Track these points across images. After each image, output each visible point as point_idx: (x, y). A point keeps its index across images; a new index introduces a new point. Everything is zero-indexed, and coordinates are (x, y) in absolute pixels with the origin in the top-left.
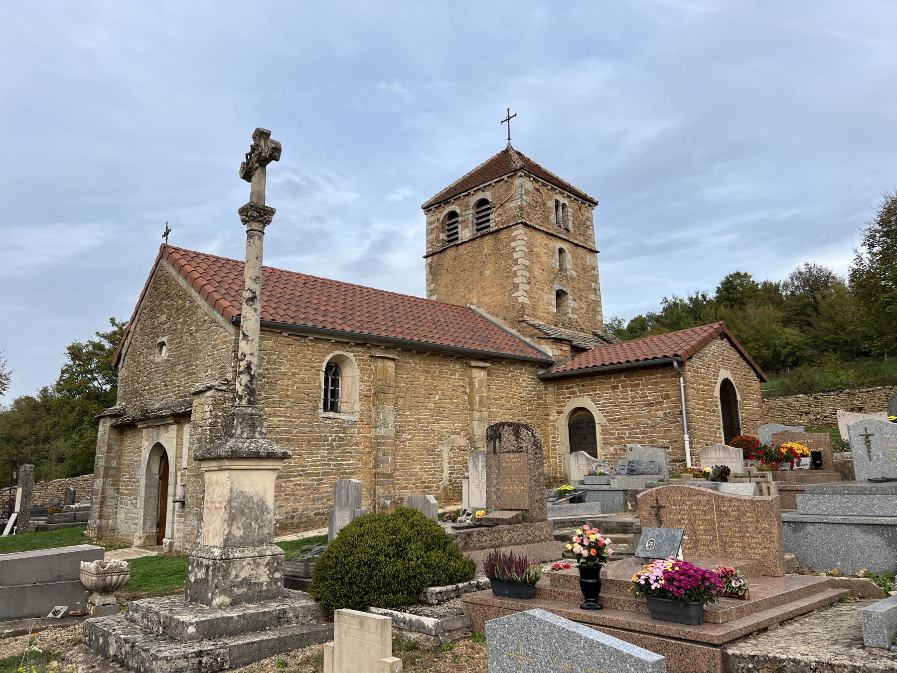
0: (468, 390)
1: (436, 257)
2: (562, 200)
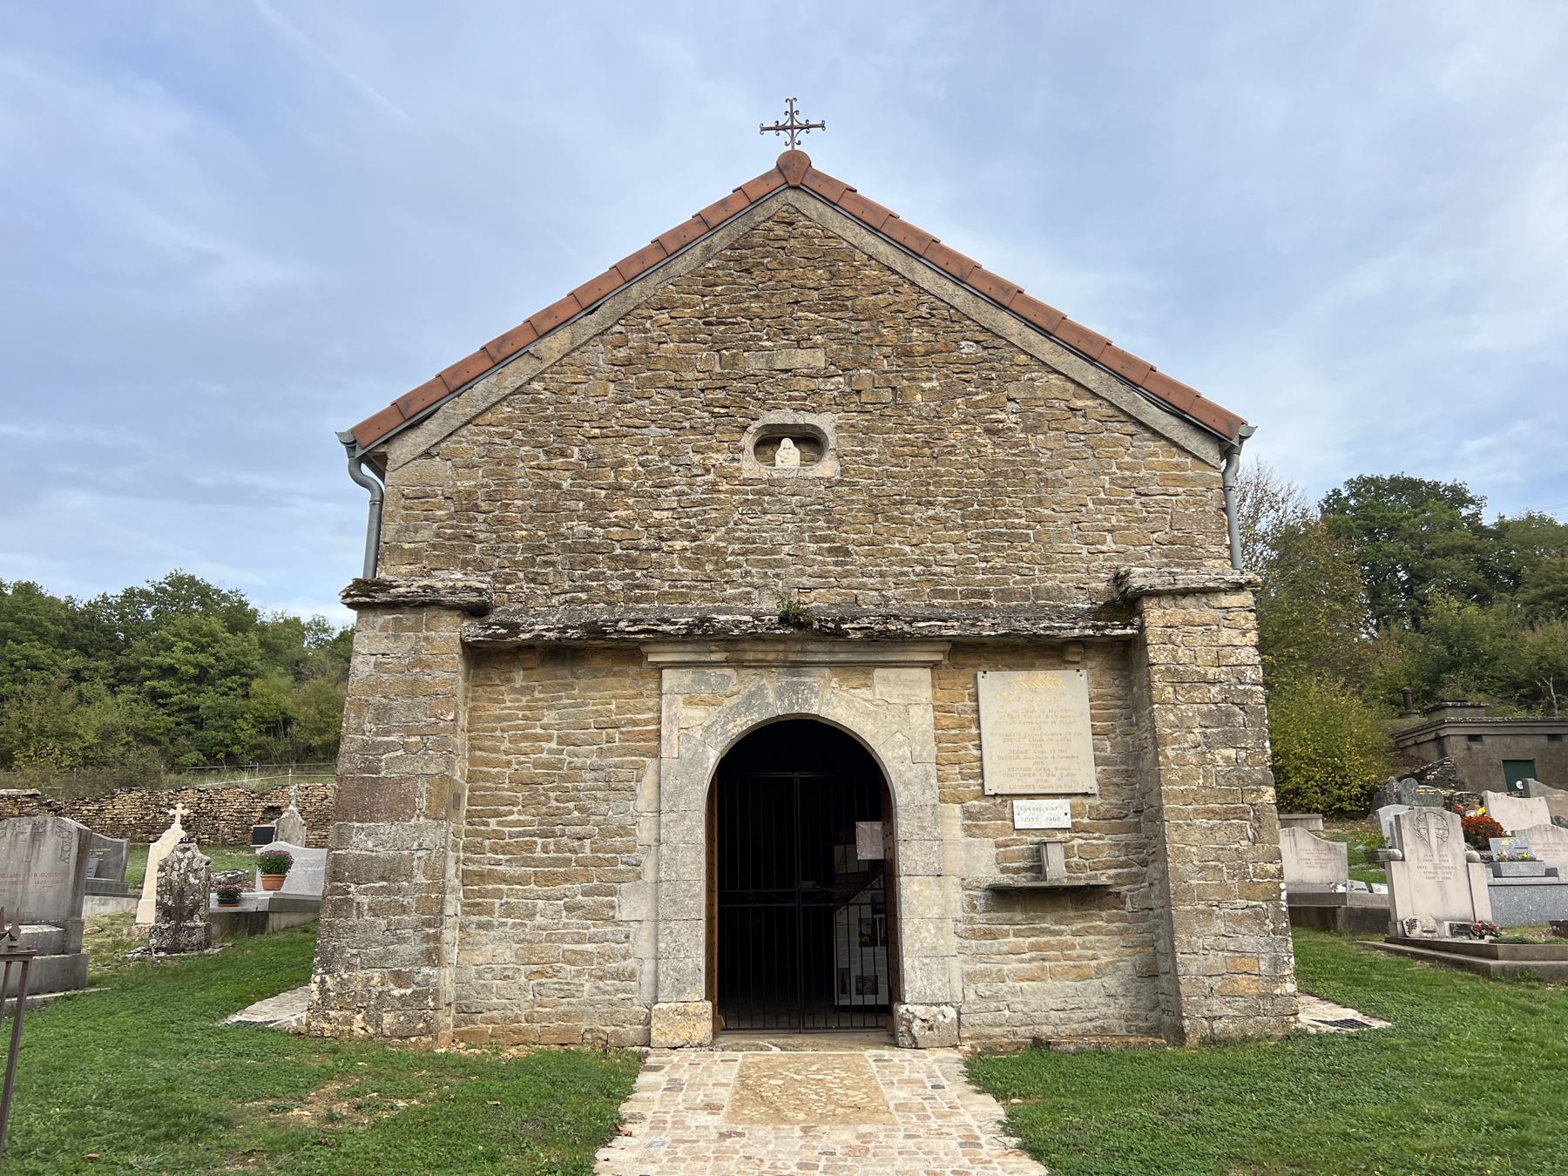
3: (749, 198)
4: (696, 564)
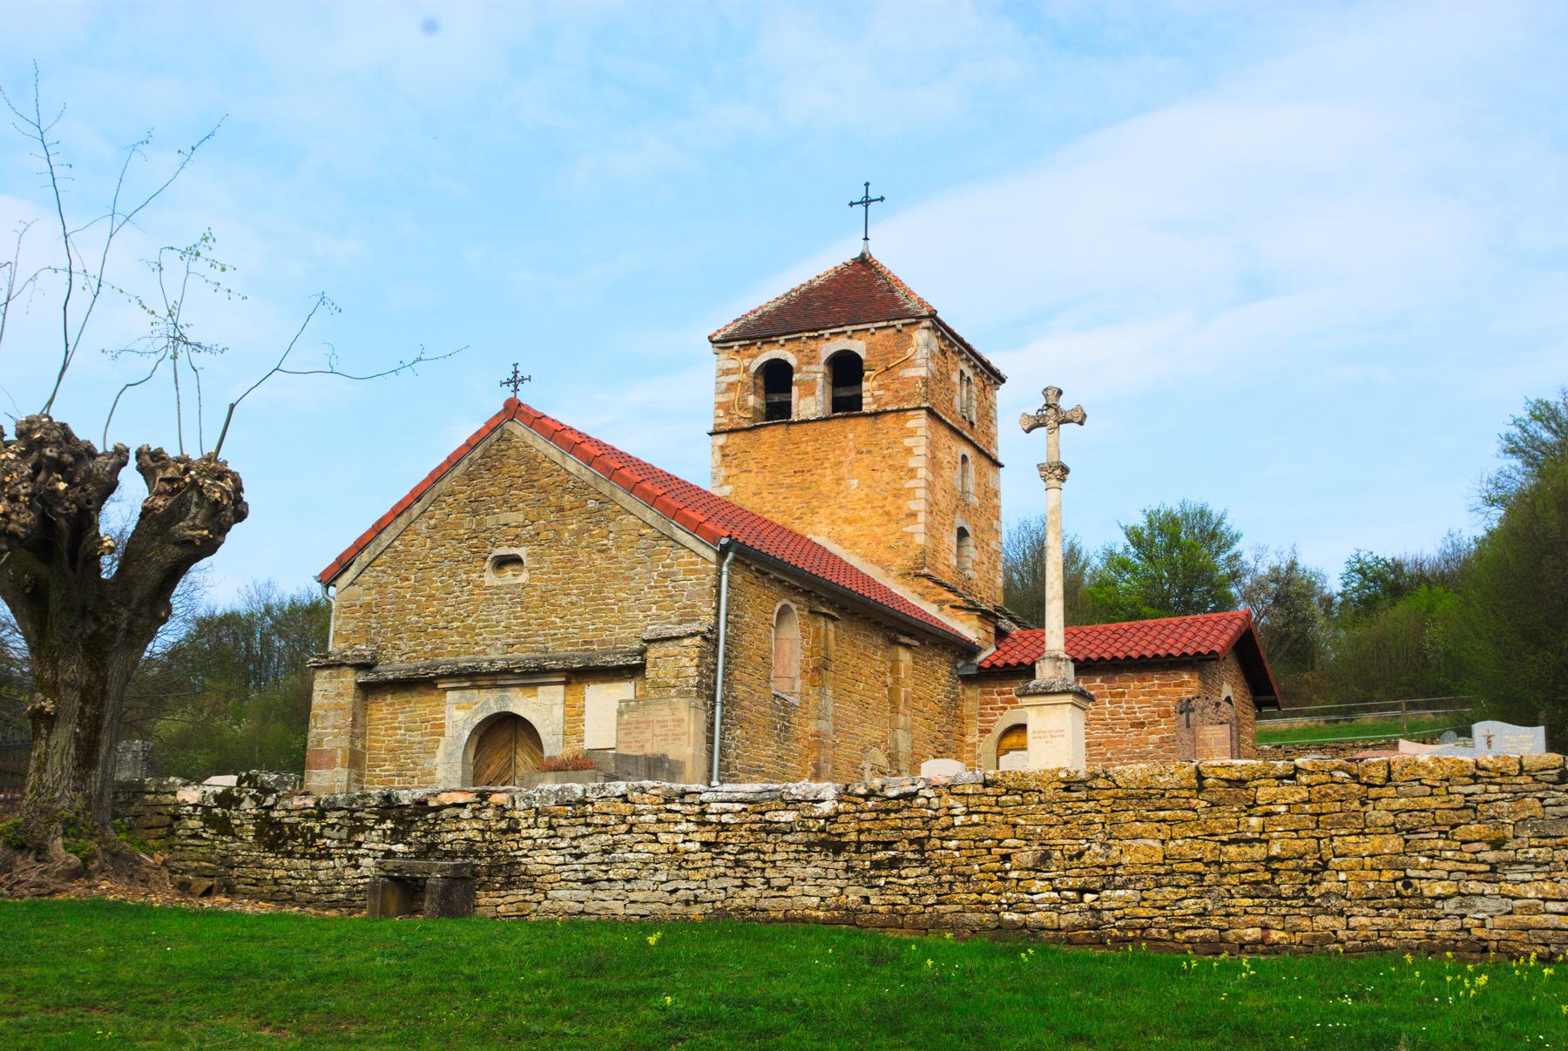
0: (889, 680)
1: (737, 438)
2: (969, 373)
4: (462, 635)
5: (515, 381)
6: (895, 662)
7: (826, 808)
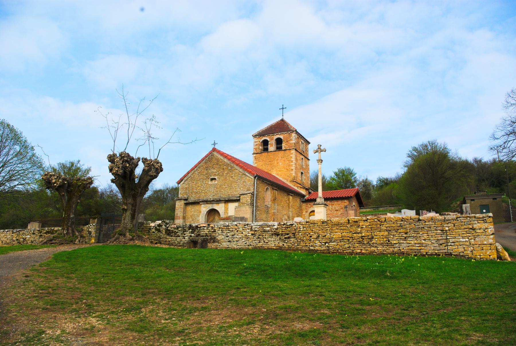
1: (258, 155)
2: (303, 142)
3: (210, 153)
5: (214, 144)
6: (289, 198)
7: (276, 227)
